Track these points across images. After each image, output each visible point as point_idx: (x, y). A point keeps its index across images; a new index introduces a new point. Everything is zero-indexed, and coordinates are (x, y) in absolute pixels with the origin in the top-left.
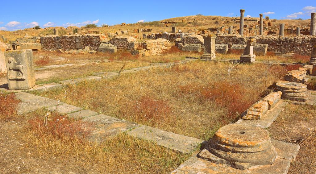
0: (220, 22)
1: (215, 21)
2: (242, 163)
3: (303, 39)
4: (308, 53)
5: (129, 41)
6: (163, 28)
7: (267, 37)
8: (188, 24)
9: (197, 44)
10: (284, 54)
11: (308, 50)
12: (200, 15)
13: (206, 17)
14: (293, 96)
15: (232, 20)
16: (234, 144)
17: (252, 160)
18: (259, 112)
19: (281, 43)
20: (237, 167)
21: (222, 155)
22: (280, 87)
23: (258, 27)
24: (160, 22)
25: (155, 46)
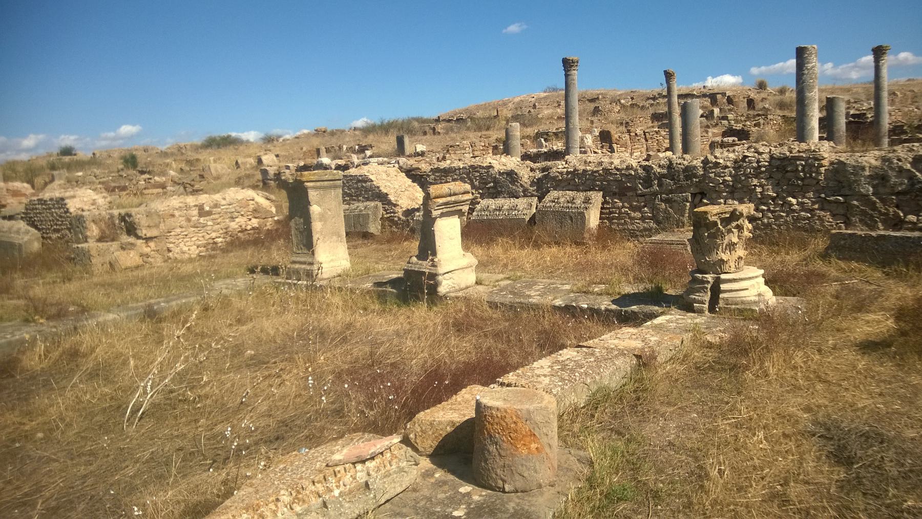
1: (592, 106)
3: (738, 164)
4: (763, 224)
5: (72, 210)
11: (762, 211)
15: (648, 99)
19: (651, 186)
25: (184, 223)
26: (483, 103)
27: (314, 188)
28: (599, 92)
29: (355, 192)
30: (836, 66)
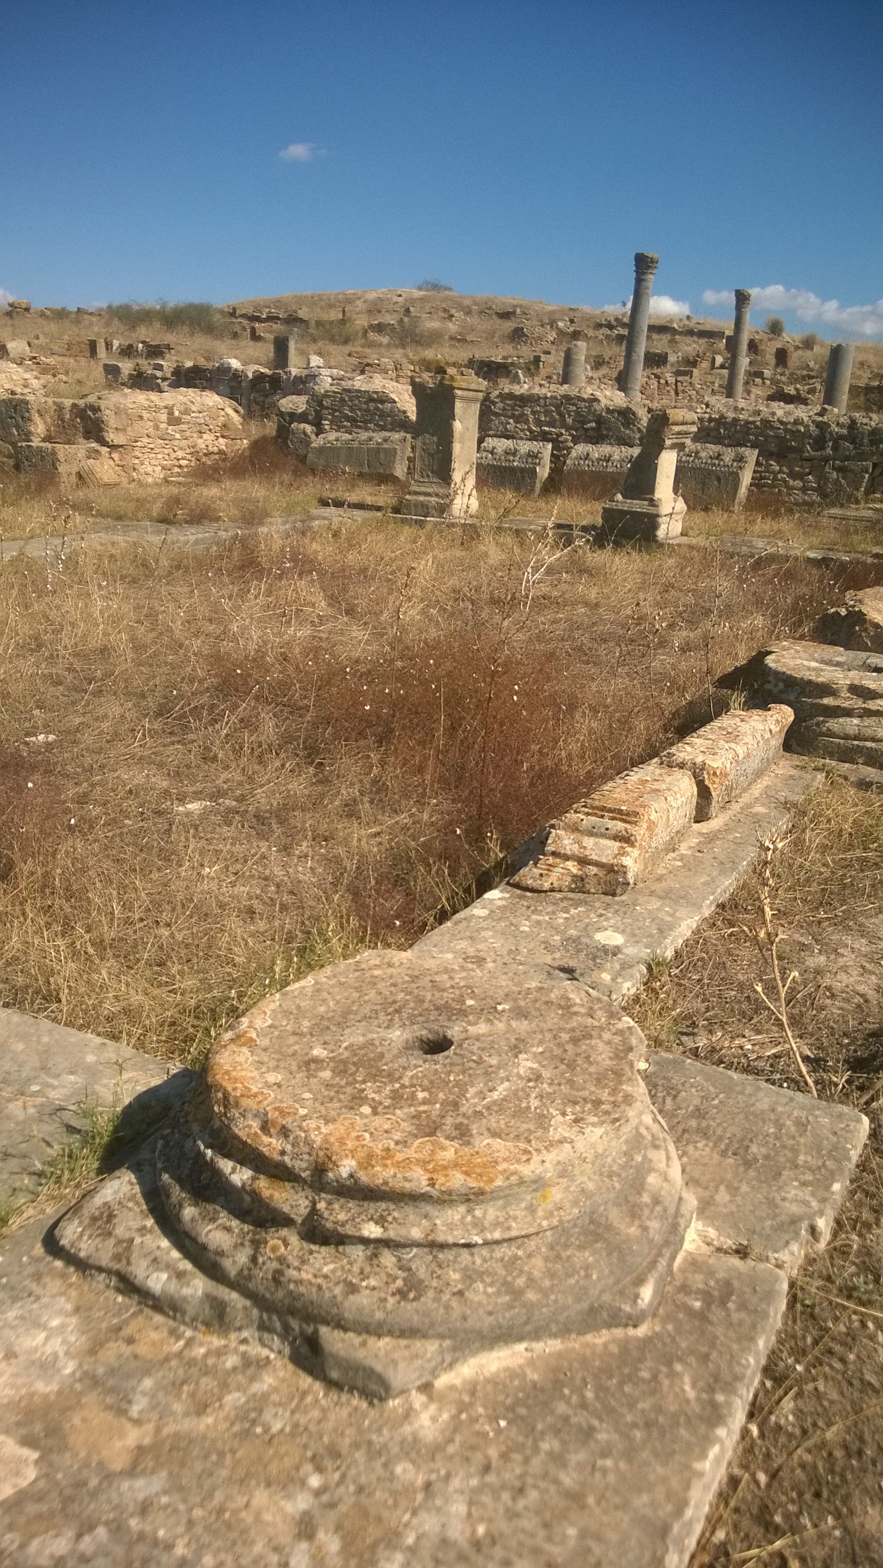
0: (538, 330)
1: (508, 326)
2: (379, 1336)
6: (234, 342)
7: (758, 413)
8: (371, 335)
9: (387, 434)
10: (833, 505)
12: (436, 287)
13: (467, 302)
14: (856, 738)
15: (599, 326)
16: (319, 1170)
17: (465, 1318)
18: (626, 839)
19: (823, 448)
20: (334, 1375)
21: (222, 1254)
22: (784, 681)
23: (722, 367)
24: (222, 312)
26: (308, 293)
27: (463, 398)
28: (515, 302)
29: (363, 416)
30: (842, 307)
